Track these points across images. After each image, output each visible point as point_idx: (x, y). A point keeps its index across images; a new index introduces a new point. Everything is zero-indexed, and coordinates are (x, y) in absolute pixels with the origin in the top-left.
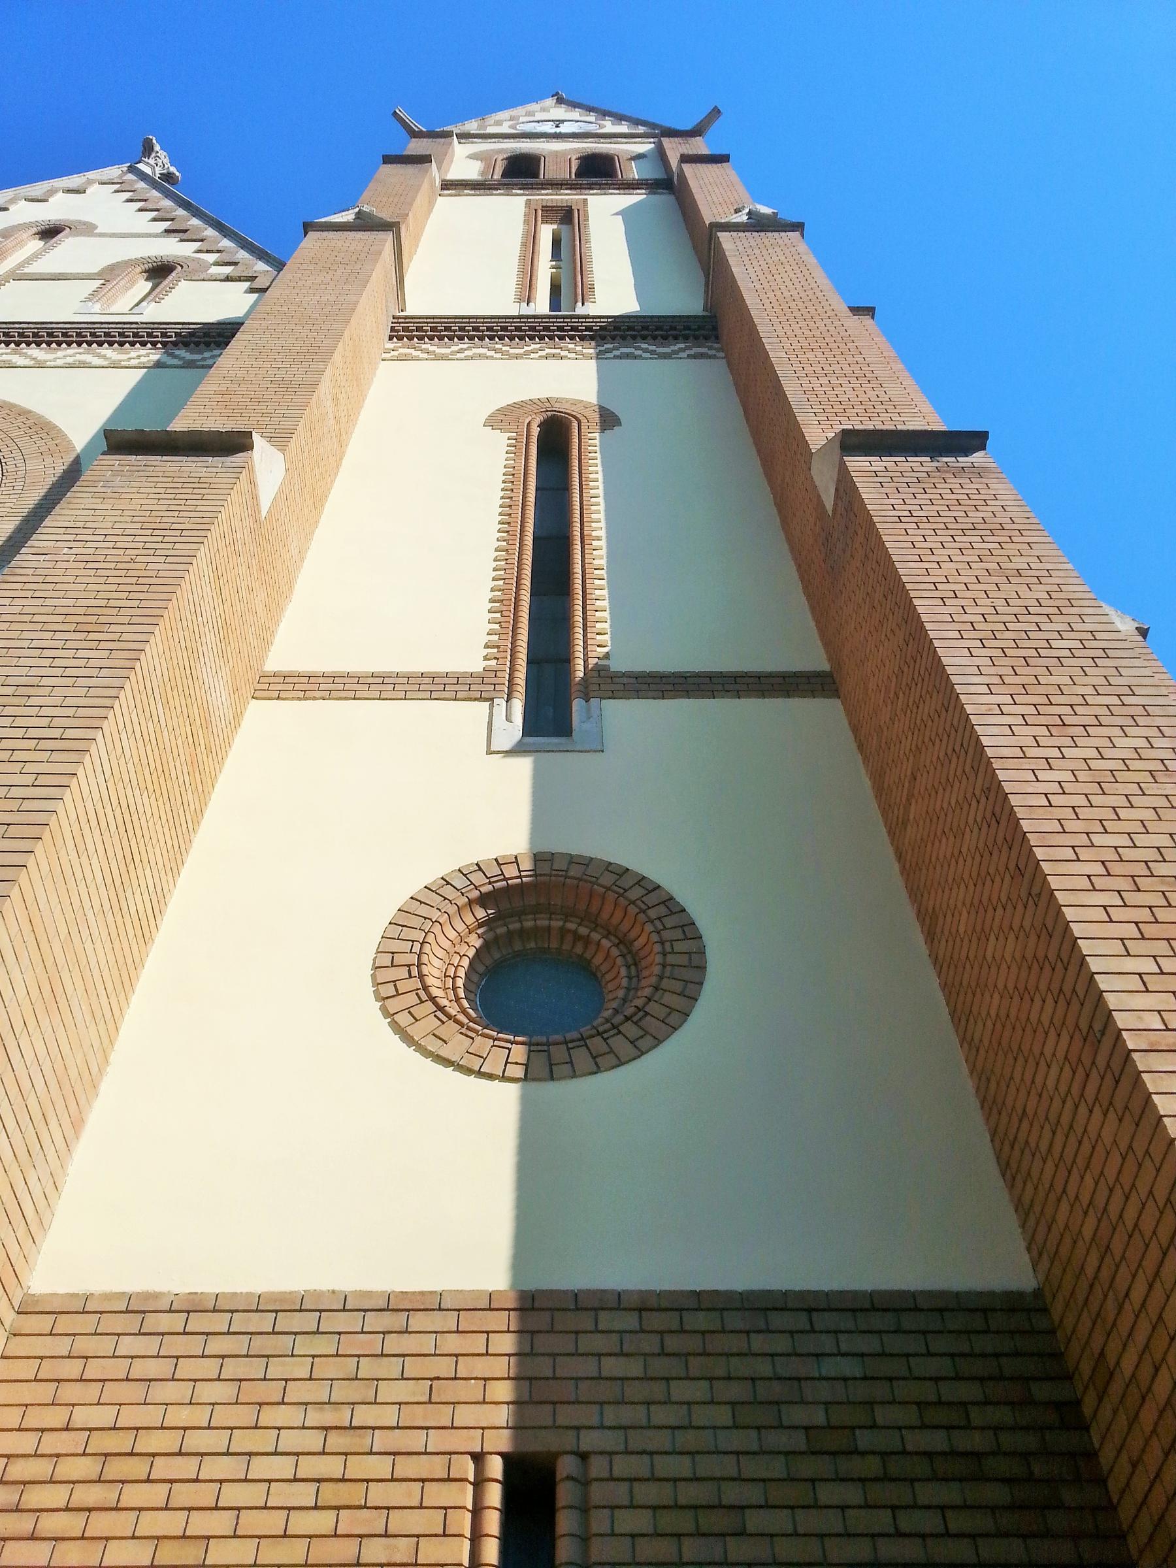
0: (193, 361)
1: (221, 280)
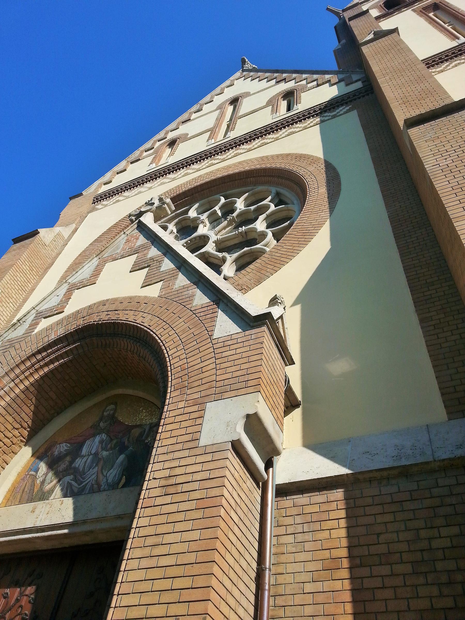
0: (335, 115)
1: (316, 87)
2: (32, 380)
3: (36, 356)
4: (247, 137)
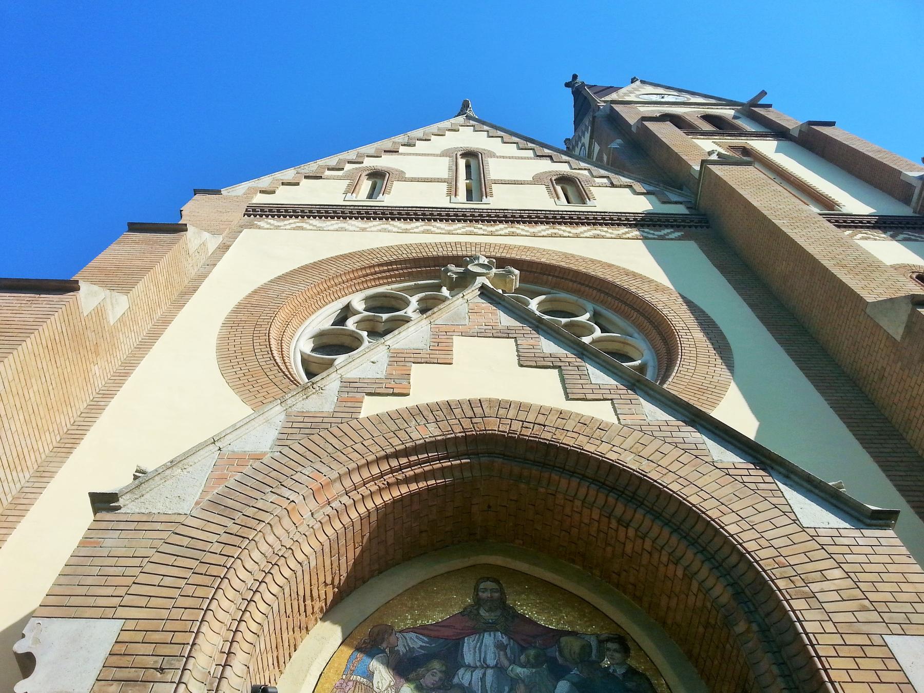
2: (378, 501)
3: (390, 460)
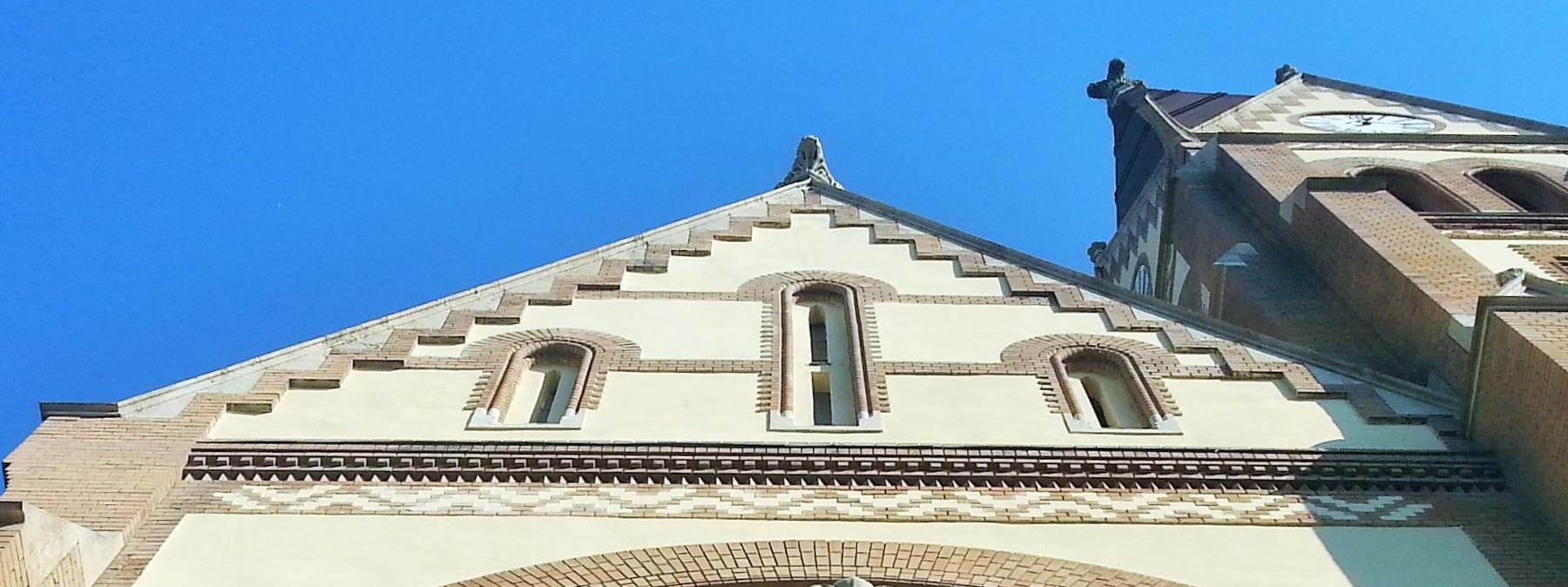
4: (429, 458)
